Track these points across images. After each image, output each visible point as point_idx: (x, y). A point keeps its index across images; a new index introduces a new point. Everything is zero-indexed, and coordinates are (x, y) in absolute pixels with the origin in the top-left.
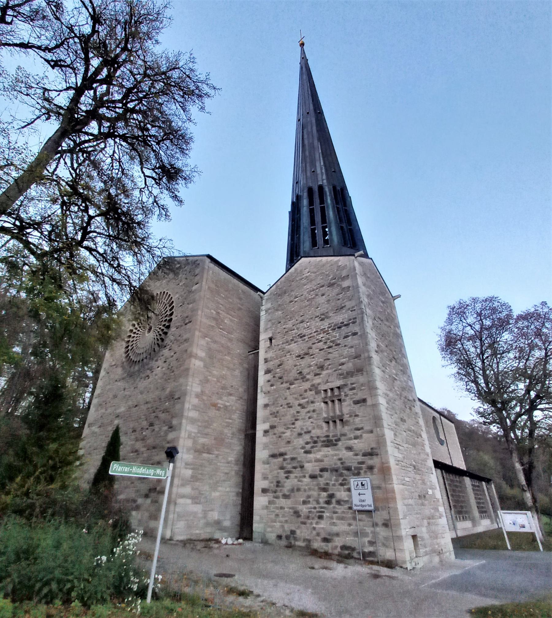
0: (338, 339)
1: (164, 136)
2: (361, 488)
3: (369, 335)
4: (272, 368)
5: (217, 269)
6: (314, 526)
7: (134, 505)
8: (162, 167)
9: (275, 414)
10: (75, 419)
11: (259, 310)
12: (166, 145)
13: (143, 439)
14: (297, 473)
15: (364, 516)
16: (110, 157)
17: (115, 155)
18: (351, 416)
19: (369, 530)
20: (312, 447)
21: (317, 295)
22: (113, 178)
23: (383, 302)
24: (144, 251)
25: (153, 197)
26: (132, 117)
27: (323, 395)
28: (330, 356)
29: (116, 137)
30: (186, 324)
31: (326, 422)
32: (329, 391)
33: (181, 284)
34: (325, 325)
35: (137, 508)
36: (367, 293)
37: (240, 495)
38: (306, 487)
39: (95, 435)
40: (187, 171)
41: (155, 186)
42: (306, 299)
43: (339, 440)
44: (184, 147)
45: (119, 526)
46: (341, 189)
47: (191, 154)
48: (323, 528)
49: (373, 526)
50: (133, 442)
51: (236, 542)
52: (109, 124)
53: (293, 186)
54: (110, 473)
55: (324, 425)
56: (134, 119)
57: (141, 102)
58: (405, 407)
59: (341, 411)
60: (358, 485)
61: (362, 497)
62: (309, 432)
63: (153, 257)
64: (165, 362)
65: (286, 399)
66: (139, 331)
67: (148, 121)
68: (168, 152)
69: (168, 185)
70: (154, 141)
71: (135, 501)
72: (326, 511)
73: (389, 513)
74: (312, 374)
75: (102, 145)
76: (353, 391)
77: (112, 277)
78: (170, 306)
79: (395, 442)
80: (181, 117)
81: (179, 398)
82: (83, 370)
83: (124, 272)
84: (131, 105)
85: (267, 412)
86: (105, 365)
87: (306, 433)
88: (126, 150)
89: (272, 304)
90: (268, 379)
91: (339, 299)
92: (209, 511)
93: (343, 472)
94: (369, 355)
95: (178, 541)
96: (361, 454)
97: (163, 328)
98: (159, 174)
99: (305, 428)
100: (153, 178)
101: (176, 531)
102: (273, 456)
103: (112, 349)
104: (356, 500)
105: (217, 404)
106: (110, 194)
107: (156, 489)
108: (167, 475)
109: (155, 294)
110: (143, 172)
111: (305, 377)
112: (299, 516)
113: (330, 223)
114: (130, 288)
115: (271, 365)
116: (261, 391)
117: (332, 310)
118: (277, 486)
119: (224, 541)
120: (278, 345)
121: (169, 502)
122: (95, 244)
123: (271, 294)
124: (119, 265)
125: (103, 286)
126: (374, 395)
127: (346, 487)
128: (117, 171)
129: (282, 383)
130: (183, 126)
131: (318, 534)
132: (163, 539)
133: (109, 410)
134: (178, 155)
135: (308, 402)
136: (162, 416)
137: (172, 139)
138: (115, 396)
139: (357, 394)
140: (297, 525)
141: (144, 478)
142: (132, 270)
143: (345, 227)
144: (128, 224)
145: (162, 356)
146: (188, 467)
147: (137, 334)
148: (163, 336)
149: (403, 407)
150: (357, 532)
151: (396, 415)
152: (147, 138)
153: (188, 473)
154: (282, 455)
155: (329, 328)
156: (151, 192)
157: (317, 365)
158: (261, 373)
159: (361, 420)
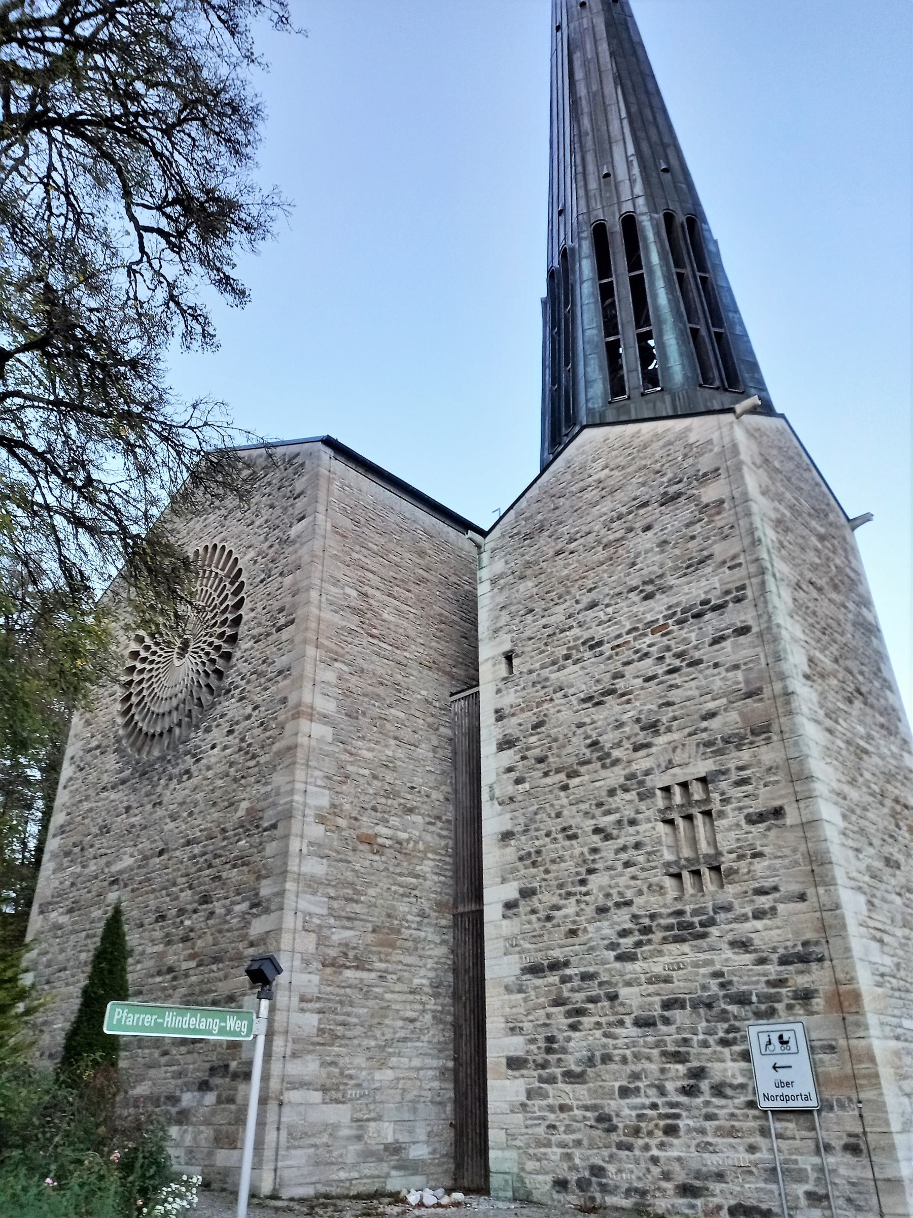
0: (696, 648)
1: (181, 112)
2: (778, 1050)
3: (784, 632)
4: (516, 732)
5: (353, 475)
6: (655, 1152)
7: (174, 1110)
8: (184, 200)
9: (530, 859)
10: (5, 893)
11: (474, 582)
12: (189, 135)
13: (185, 939)
14: (600, 1013)
15: (790, 1127)
16: (41, 182)
17: (54, 174)
18: (741, 857)
19: (807, 1162)
20: (639, 944)
21: (630, 530)
22: (53, 239)
23: (822, 538)
24: (153, 439)
25: (165, 285)
26: (90, 62)
27: (660, 800)
28: (674, 695)
29: (51, 123)
30: (279, 630)
31: (672, 875)
32: (677, 790)
33: (257, 523)
34: (657, 609)
35: (183, 1118)
36: (773, 515)
37: (450, 1075)
38: (628, 1052)
39: (59, 933)
40: (251, 205)
41: (169, 254)
42: (600, 542)
43: (712, 922)
44: (240, 136)
45: (138, 1165)
46: (688, 219)
47: (259, 154)
48: (679, 1159)
49: (818, 1152)
50: (160, 948)
51: (445, 1200)
52: (29, 89)
53: (550, 222)
54: (106, 1031)
55: (669, 882)
56: (96, 68)
57: (112, 17)
58: (897, 826)
59: (714, 843)
60: (770, 1043)
61: (783, 1075)
62: (628, 903)
63: (179, 453)
64: (230, 732)
65: (558, 815)
66: (154, 653)
67: (136, 70)
68: (197, 155)
69: (204, 249)
70: (155, 128)
71: (173, 1099)
72: (684, 1114)
73: (861, 1116)
74: (627, 745)
75: (17, 151)
76: (744, 788)
77: (72, 513)
78: (232, 583)
79: (872, 923)
80: (225, 52)
81: (274, 826)
82: (17, 765)
83: (103, 497)
84: (85, 29)
85: (510, 852)
86: (72, 749)
87: (618, 905)
88: (81, 159)
89: (507, 563)
90: (507, 764)
91: (693, 538)
92: (368, 1120)
93: (729, 1008)
94: (785, 687)
95: (292, 1199)
96: (776, 960)
97: (217, 642)
98: (176, 221)
99: (614, 892)
100: (160, 232)
101: (286, 1174)
102: (535, 970)
103: (88, 708)
104: (766, 1083)
105: (376, 835)
106: (48, 287)
107: (227, 1066)
108: (254, 1032)
109: (191, 555)
110: (133, 218)
111: (608, 755)
112: (613, 1129)
113: (660, 322)
114: (123, 540)
115: (511, 726)
116: (492, 798)
117: (676, 568)
118: (549, 1051)
119: (413, 1198)
120: (530, 672)
121: (263, 1101)
122: (21, 428)
123: (503, 536)
124: (89, 481)
125: (52, 538)
126: (803, 798)
127: (737, 1048)
128: (62, 220)
129: (546, 774)
130: (233, 75)
131: (666, 1176)
132: (252, 1195)
133: (92, 867)
134: (224, 162)
135: (619, 822)
136: (233, 875)
137: (205, 116)
138: (105, 829)
139: (756, 797)
140: (606, 1153)
141: (194, 1041)
142: (126, 493)
143: (703, 332)
144: (103, 367)
145: (222, 716)
146: (310, 1005)
147: (152, 662)
148: (220, 664)
149: (892, 827)
150: (774, 1169)
151: (871, 851)
152: (136, 120)
153: (310, 1021)
154: (554, 966)
155: (666, 617)
156: (158, 273)
157: (638, 720)
158: (488, 748)
159: (769, 867)
